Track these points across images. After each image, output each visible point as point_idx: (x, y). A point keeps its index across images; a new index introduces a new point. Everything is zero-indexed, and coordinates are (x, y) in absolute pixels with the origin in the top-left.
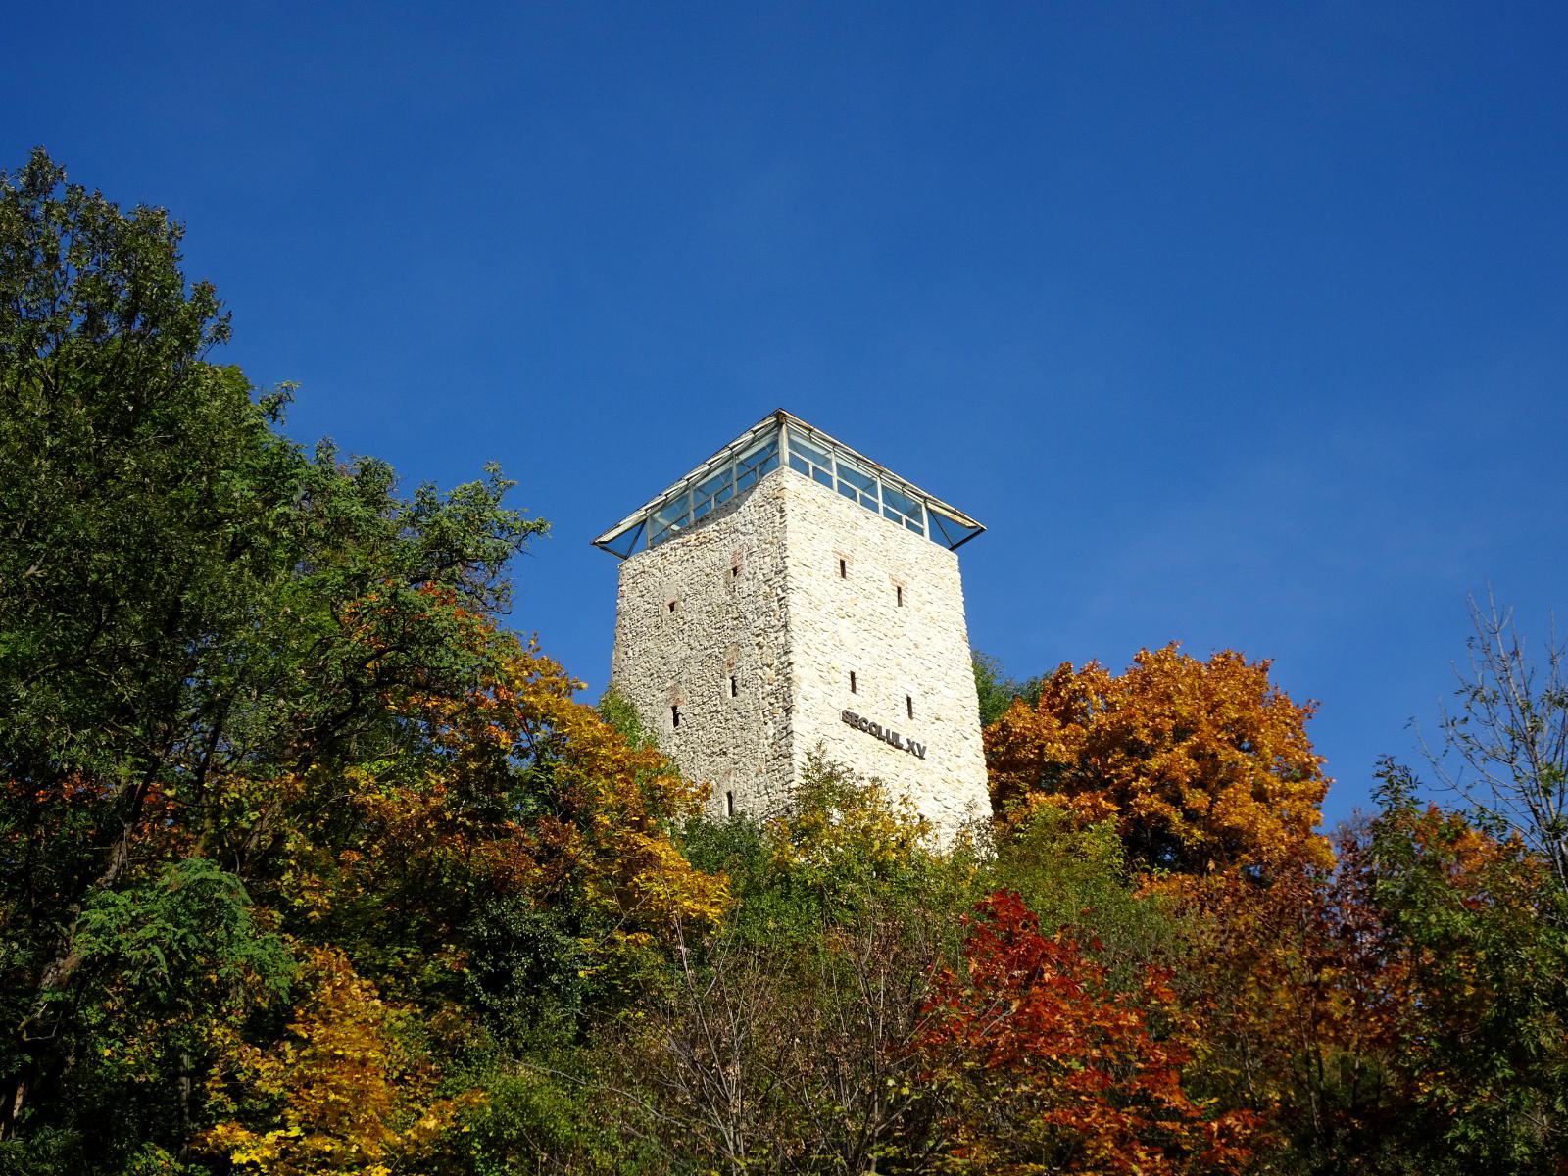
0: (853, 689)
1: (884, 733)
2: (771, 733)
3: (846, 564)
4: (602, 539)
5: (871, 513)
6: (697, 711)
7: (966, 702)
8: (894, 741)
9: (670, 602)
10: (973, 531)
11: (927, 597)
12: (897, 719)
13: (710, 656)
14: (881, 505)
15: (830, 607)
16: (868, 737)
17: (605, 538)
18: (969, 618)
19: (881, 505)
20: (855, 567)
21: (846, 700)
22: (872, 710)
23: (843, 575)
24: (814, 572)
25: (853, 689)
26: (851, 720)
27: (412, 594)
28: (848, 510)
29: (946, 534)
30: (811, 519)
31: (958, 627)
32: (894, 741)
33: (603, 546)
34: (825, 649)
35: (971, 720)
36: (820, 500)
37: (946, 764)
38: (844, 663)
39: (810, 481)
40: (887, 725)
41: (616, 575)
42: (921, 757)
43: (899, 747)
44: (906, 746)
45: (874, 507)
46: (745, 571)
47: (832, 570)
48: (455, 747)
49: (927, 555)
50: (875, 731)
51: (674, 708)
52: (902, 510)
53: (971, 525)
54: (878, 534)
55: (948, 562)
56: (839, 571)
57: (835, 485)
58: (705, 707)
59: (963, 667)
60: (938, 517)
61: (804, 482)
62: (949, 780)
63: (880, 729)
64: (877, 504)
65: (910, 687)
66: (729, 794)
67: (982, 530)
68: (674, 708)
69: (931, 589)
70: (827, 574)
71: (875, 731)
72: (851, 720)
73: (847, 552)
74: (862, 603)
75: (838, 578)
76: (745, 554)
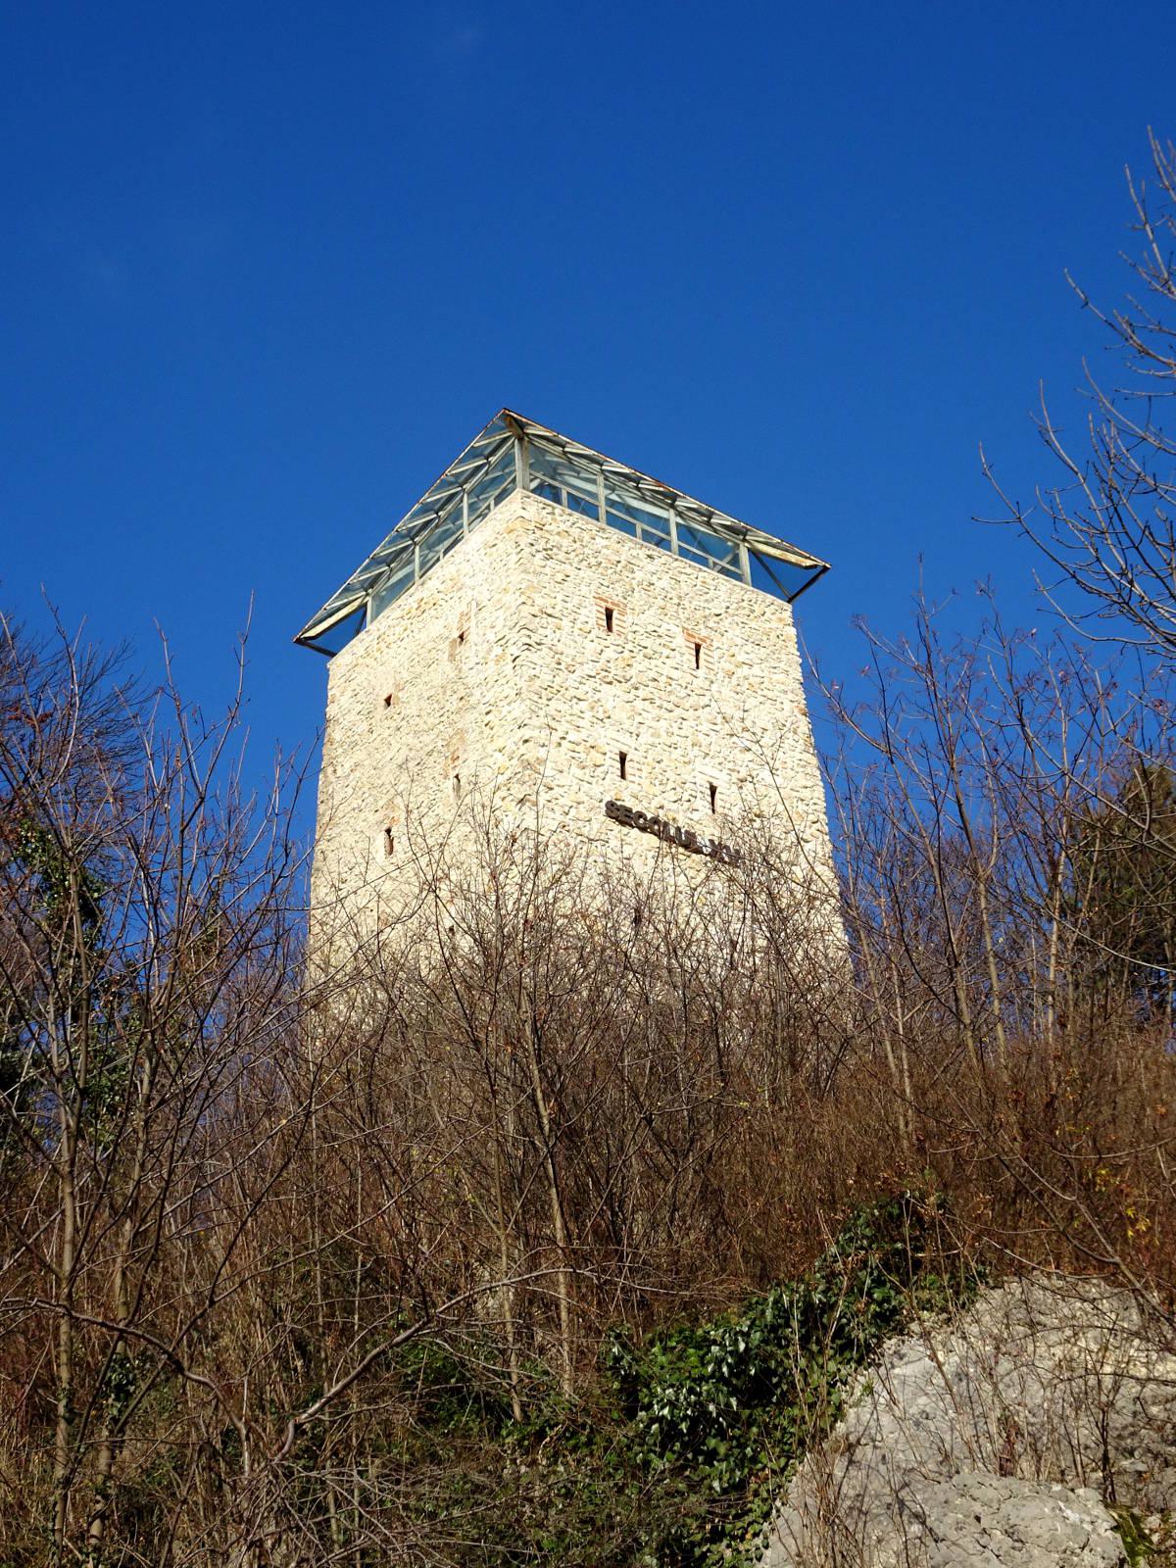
0: (623, 776)
1: (672, 832)
3: (615, 614)
4: (306, 635)
7: (806, 794)
9: (386, 696)
10: (814, 572)
11: (741, 657)
13: (429, 754)
18: (809, 682)
20: (629, 618)
21: (612, 788)
22: (655, 803)
23: (610, 628)
24: (566, 623)
25: (623, 776)
26: (621, 815)
27: (511, 1339)
29: (768, 575)
30: (562, 556)
31: (790, 696)
34: (581, 723)
36: (575, 532)
38: (611, 739)
41: (324, 676)
43: (698, 851)
46: (471, 638)
47: (592, 621)
49: (745, 604)
51: (388, 831)
52: (700, 547)
53: (809, 563)
54: (666, 577)
55: (776, 616)
56: (605, 623)
57: (639, 531)
60: (762, 557)
61: (549, 510)
63: (691, 836)
64: (670, 542)
65: (716, 773)
67: (825, 569)
68: (388, 831)
69: (749, 647)
72: (621, 815)
73: (616, 600)
74: (640, 664)
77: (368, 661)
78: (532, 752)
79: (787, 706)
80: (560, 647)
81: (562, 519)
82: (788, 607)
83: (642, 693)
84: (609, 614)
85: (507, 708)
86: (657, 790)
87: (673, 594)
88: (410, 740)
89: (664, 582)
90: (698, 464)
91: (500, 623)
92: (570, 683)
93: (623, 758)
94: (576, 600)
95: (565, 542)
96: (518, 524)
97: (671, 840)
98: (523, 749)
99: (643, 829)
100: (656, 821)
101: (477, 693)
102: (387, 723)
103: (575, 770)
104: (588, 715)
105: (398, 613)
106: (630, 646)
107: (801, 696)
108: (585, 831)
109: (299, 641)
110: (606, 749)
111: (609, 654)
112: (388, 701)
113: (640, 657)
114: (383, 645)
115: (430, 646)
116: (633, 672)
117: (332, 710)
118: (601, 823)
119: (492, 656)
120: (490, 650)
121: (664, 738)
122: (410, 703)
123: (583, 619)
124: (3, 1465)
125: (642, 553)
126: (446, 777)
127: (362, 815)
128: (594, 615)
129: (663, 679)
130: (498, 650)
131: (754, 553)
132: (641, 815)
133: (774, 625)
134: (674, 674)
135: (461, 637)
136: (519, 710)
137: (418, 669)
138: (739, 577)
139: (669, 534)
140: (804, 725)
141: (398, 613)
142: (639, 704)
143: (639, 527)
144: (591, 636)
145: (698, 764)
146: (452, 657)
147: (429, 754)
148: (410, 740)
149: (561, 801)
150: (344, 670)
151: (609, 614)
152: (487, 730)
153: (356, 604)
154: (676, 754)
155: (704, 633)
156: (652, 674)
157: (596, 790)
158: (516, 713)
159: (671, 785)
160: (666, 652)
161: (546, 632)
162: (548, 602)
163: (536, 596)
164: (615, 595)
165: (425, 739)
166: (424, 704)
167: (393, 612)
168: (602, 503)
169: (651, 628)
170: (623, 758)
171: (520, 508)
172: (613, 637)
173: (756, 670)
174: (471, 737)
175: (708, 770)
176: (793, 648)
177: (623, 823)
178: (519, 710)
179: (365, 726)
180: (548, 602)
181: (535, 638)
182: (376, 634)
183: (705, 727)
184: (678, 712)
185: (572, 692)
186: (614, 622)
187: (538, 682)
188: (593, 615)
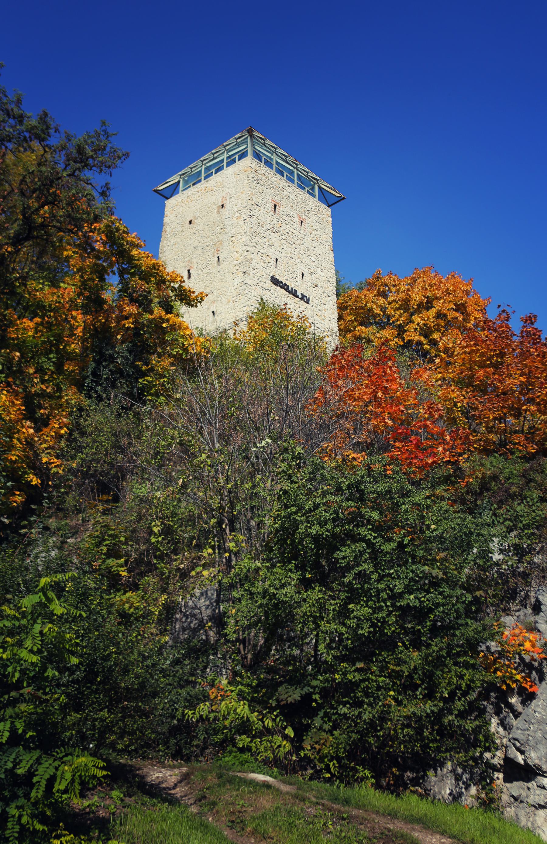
2: (235, 284)
5: (291, 184)
6: (200, 272)
7: (330, 279)
8: (294, 293)
11: (314, 227)
12: (297, 284)
13: (207, 246)
14: (296, 181)
15: (268, 227)
16: (283, 291)
17: (160, 188)
18: (334, 239)
19: (296, 181)
20: (282, 209)
21: (272, 271)
22: (285, 278)
24: (262, 208)
26: (275, 281)
28: (283, 182)
29: (324, 197)
30: (262, 183)
32: (294, 293)
33: (156, 191)
35: (332, 288)
37: (319, 307)
38: (273, 253)
39: (262, 165)
40: (292, 285)
42: (308, 303)
43: (297, 297)
44: (300, 296)
45: (292, 181)
46: (227, 206)
48: (142, 566)
50: (285, 287)
51: (189, 271)
52: (304, 183)
55: (326, 212)
58: (204, 270)
59: (330, 262)
62: (319, 315)
63: (296, 291)
65: (304, 269)
66: (213, 312)
67: (344, 198)
68: (189, 271)
70: (268, 211)
71: (285, 287)
73: (278, 201)
75: (272, 213)
76: (228, 198)
77: (182, 204)
78: (249, 256)
79: (327, 247)
80: (260, 218)
81: (263, 169)
82: (330, 210)
83: (284, 237)
84: (275, 206)
85: (240, 237)
86: (286, 273)
87: (295, 201)
88: (199, 238)
89: (293, 197)
90: (312, 156)
91: (239, 205)
92: (262, 231)
93: (277, 260)
94: (266, 200)
95: (263, 178)
96: (249, 169)
97: (289, 292)
98: (246, 253)
99: (281, 287)
100: (286, 285)
101: (228, 228)
102: (189, 230)
103: (262, 263)
104: (267, 243)
105: (196, 190)
106: (281, 219)
107: (331, 244)
108: (264, 286)
109: (154, 191)
110: (272, 257)
111: (275, 222)
112: (190, 222)
113: (284, 223)
114: (189, 201)
115: (210, 205)
116: (282, 229)
117: (166, 220)
118: (269, 284)
119: (235, 216)
120: (234, 214)
121: (289, 255)
122: (199, 224)
123: (267, 207)
124: (546, 599)
125: (287, 185)
126: (214, 256)
127: (178, 262)
128: (271, 206)
129: (290, 233)
130: (237, 215)
131: (320, 187)
132: (281, 282)
133: (325, 216)
134: (294, 231)
135: (223, 206)
136: (245, 239)
137: (204, 213)
138: (314, 196)
139: (294, 177)
140: (331, 256)
141: (196, 190)
142: (282, 241)
143: (285, 173)
144: (270, 214)
145: (299, 265)
146: (218, 212)
147: (207, 246)
148: (199, 238)
149: (258, 274)
150: (172, 205)
151: (275, 206)
152: (231, 243)
153: (176, 181)
154: (292, 261)
155: (304, 217)
156: (287, 231)
157: (268, 272)
158: (244, 240)
159: (290, 272)
160: (292, 223)
161: (256, 212)
162: (257, 200)
163: (253, 197)
164: (277, 199)
165: (206, 240)
166: (206, 227)
167: (193, 190)
168: (274, 163)
169: (288, 213)
170: (277, 260)
171: (249, 162)
172: (276, 216)
173: (318, 233)
174: (225, 244)
175: (302, 268)
176: (330, 224)
177: (275, 284)
178: (245, 239)
179: (180, 229)
180: (257, 200)
181: (252, 213)
182: (187, 195)
183: (302, 252)
184: (294, 245)
185: (263, 235)
186: (277, 210)
187: (252, 230)
188: (270, 206)
